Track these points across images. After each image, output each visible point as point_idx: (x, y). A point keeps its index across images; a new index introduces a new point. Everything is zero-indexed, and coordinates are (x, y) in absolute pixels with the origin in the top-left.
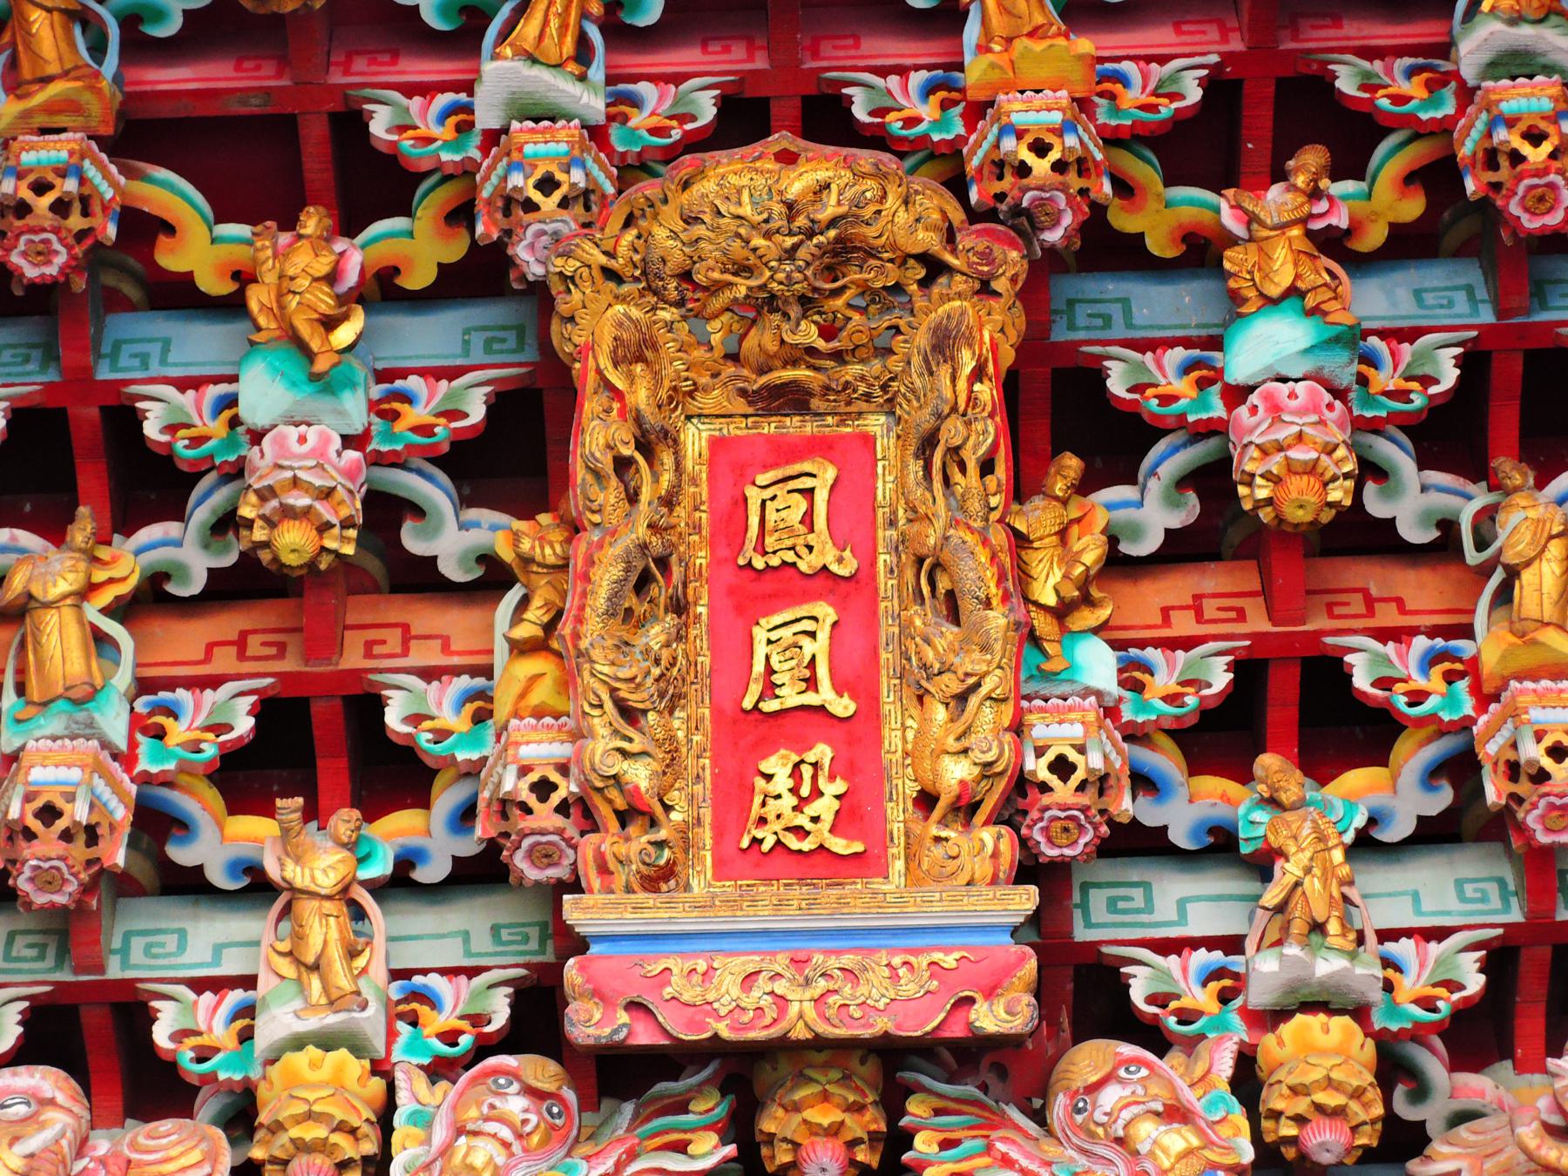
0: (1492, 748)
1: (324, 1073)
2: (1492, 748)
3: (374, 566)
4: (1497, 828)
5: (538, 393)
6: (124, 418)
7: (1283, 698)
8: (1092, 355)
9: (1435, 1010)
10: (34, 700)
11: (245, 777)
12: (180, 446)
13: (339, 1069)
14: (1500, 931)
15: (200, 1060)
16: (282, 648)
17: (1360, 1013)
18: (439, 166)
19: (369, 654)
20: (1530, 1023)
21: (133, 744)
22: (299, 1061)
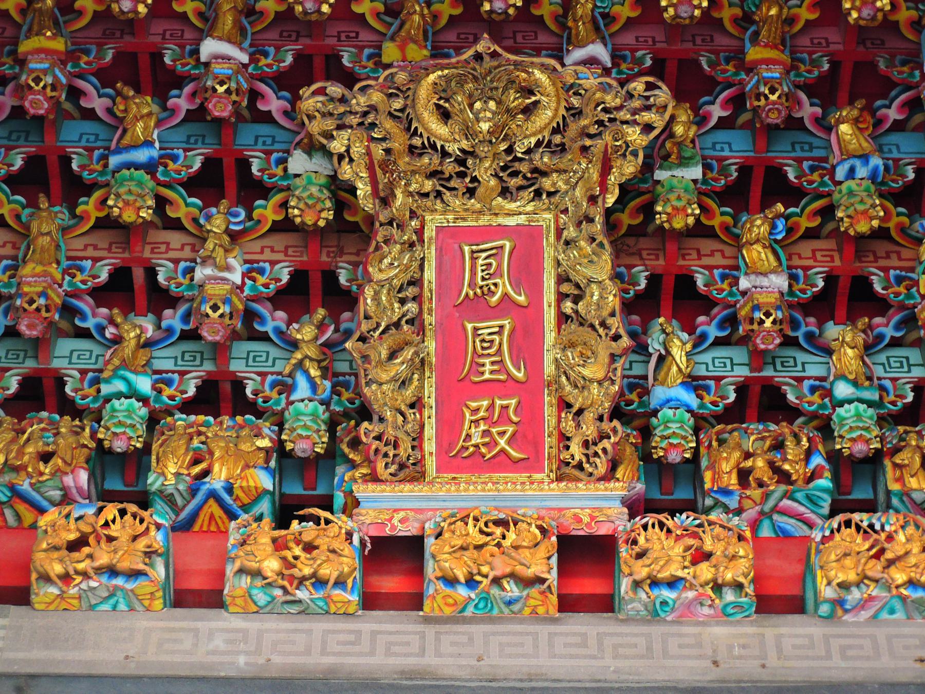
0: (743, 313)
1: (853, 413)
2: (743, 313)
3: (157, 220)
4: (744, 341)
5: (220, 161)
6: (244, 164)
7: (316, 284)
8: (60, 147)
9: (896, 406)
10: (55, 260)
11: (100, 295)
12: (265, 177)
13: (131, 405)
14: (742, 379)
15: (264, 402)
16: (302, 252)
17: (145, 401)
18: (190, 75)
19: (152, 252)
20: (752, 411)
21: (244, 283)
22: (116, 403)
